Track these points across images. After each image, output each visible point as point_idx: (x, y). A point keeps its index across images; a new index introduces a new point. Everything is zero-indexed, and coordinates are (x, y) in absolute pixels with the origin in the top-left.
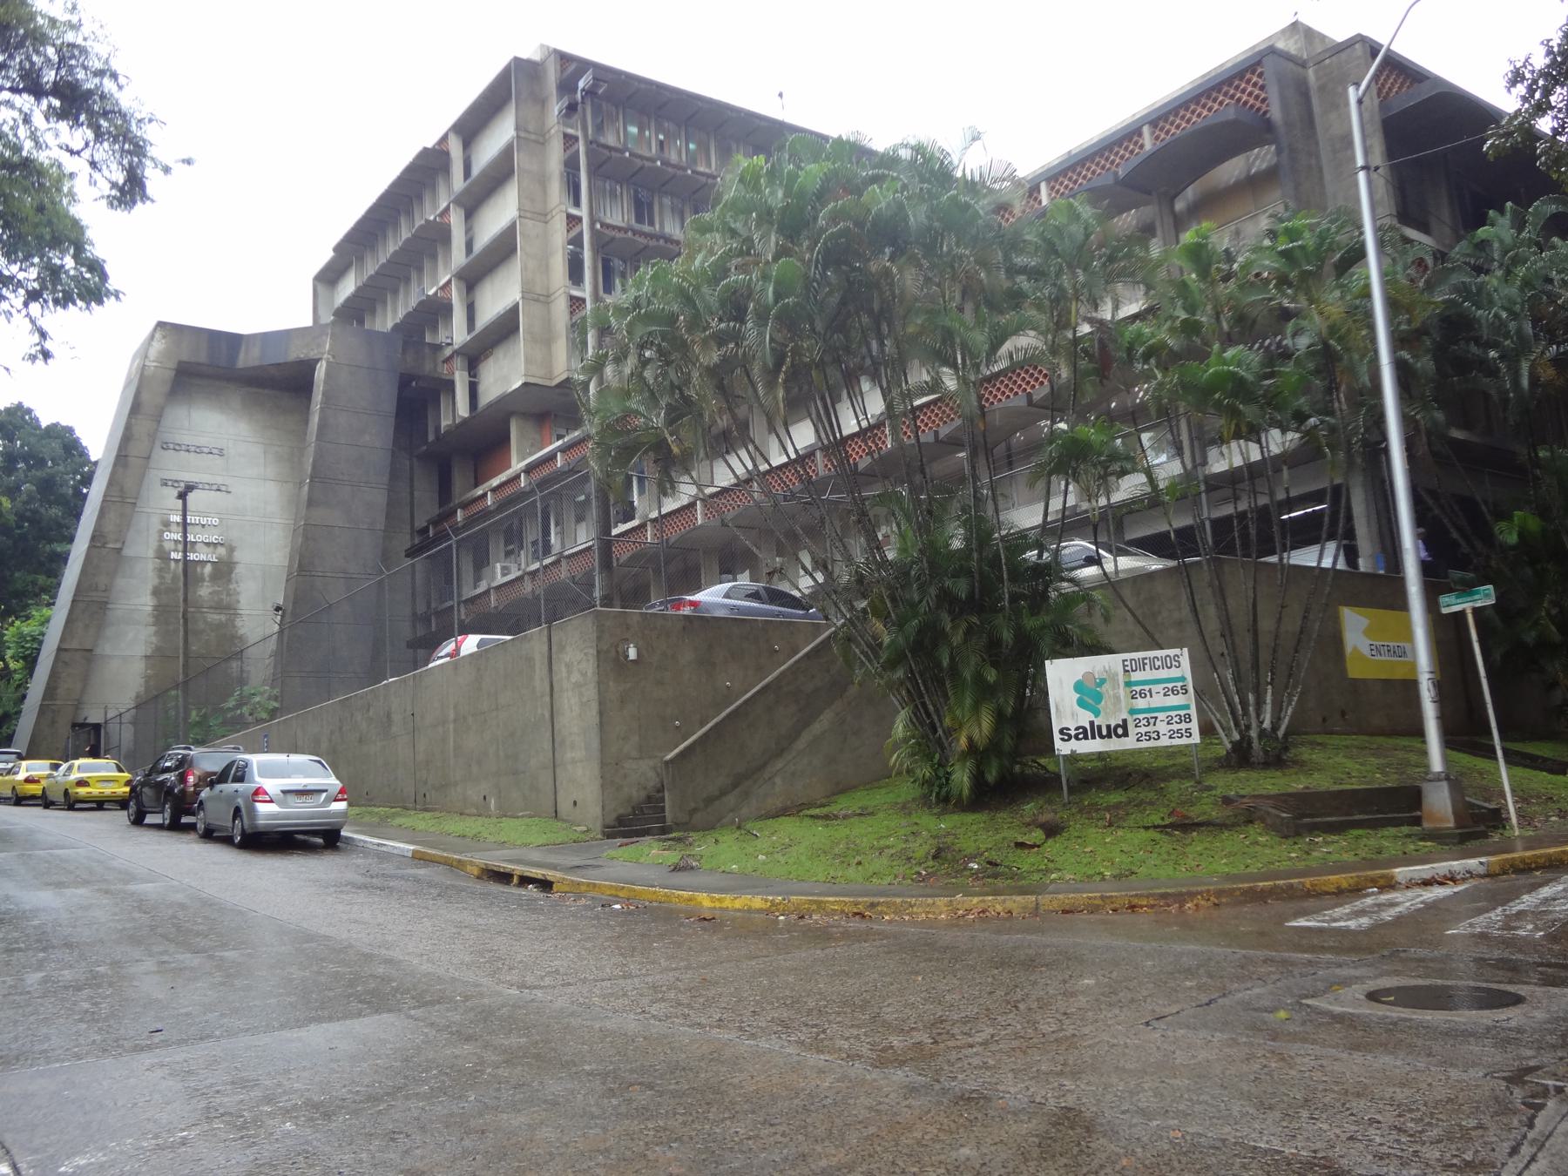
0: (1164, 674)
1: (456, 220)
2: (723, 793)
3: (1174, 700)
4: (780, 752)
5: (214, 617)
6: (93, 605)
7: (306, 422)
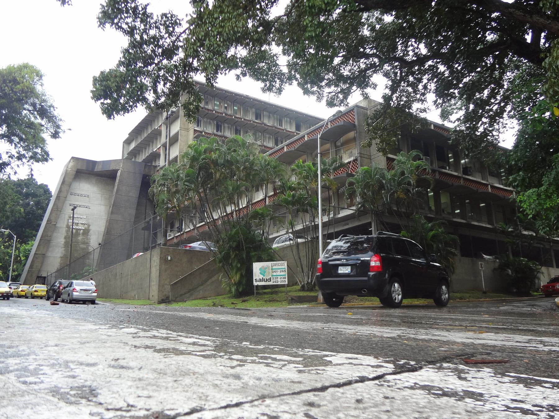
0: (280, 267)
1: (163, 129)
2: (185, 294)
3: (282, 273)
4: (202, 285)
5: (82, 246)
6: (46, 241)
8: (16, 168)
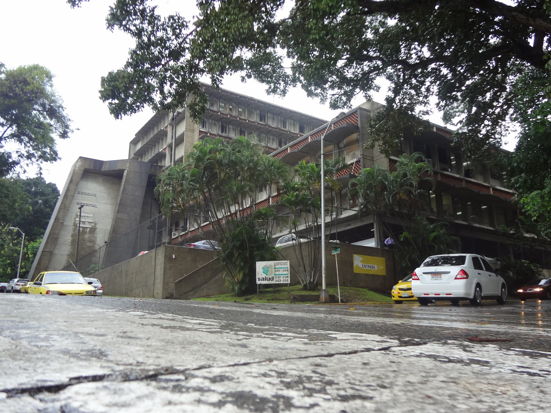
1: (169, 130)
2: (189, 291)
4: (206, 283)
5: (89, 244)
6: (54, 239)
7: (120, 187)
8: (25, 167)
